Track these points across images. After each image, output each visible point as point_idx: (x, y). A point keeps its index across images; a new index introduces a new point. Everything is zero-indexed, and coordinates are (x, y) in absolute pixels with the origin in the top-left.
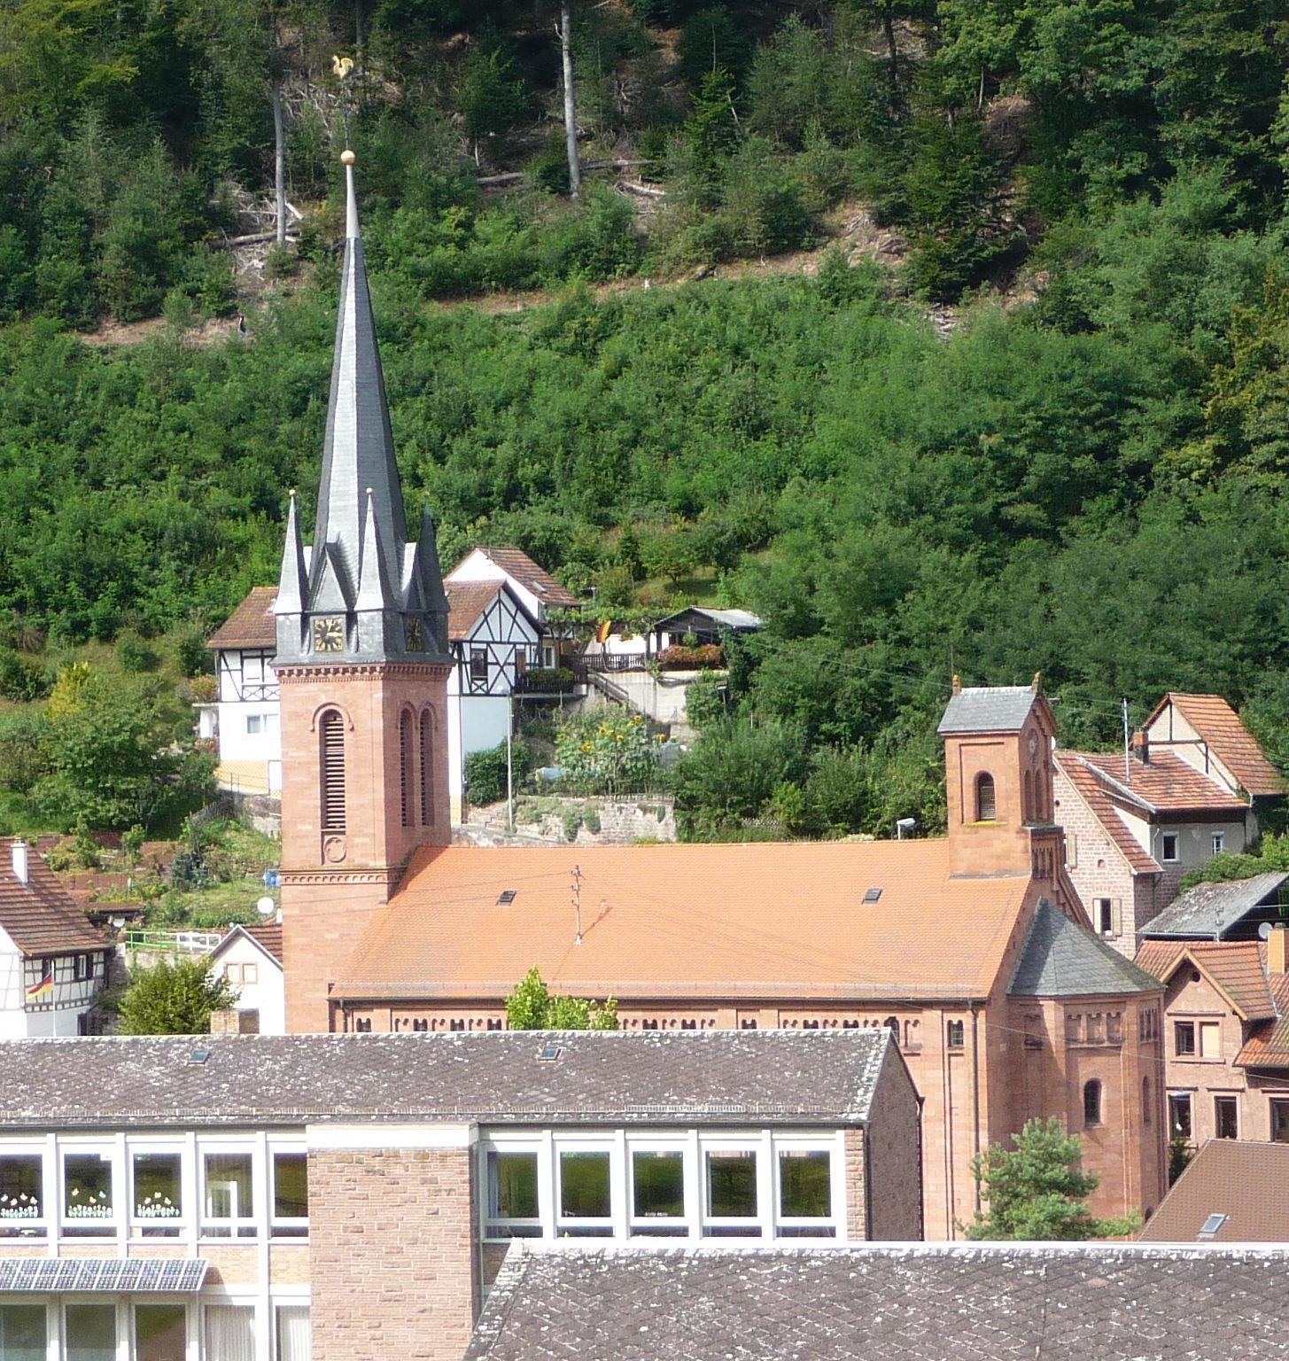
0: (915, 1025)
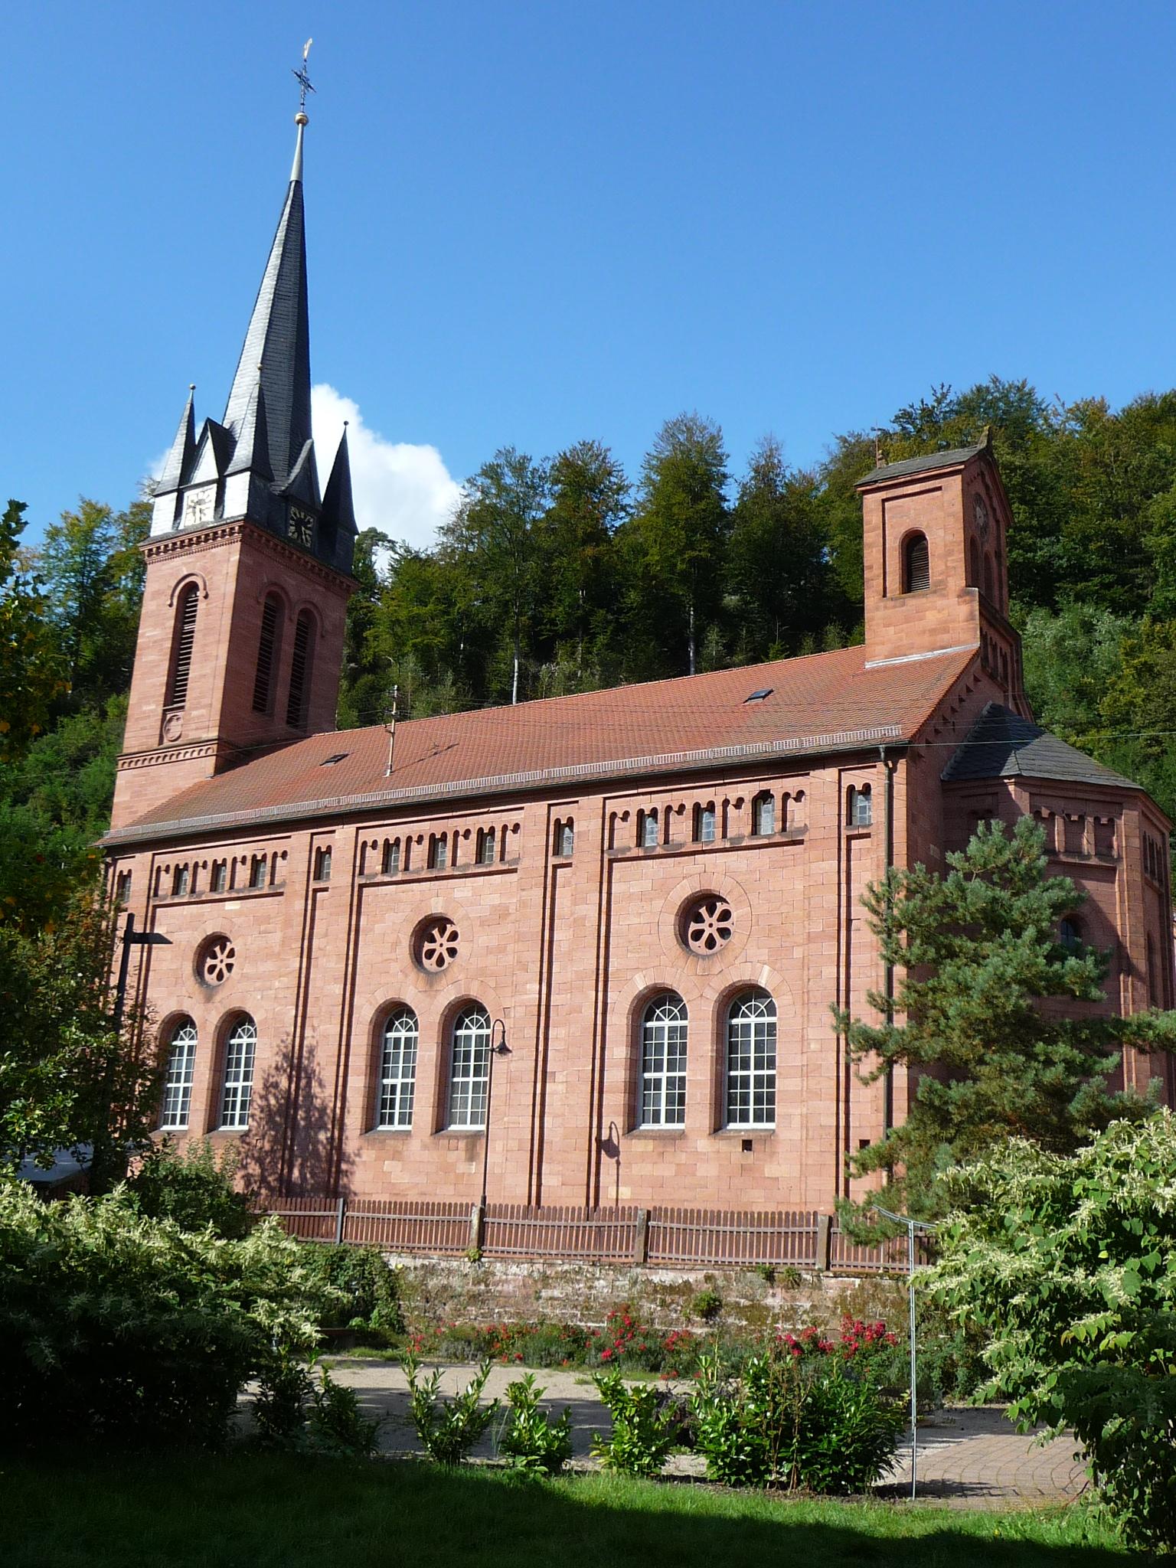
0: (798, 799)
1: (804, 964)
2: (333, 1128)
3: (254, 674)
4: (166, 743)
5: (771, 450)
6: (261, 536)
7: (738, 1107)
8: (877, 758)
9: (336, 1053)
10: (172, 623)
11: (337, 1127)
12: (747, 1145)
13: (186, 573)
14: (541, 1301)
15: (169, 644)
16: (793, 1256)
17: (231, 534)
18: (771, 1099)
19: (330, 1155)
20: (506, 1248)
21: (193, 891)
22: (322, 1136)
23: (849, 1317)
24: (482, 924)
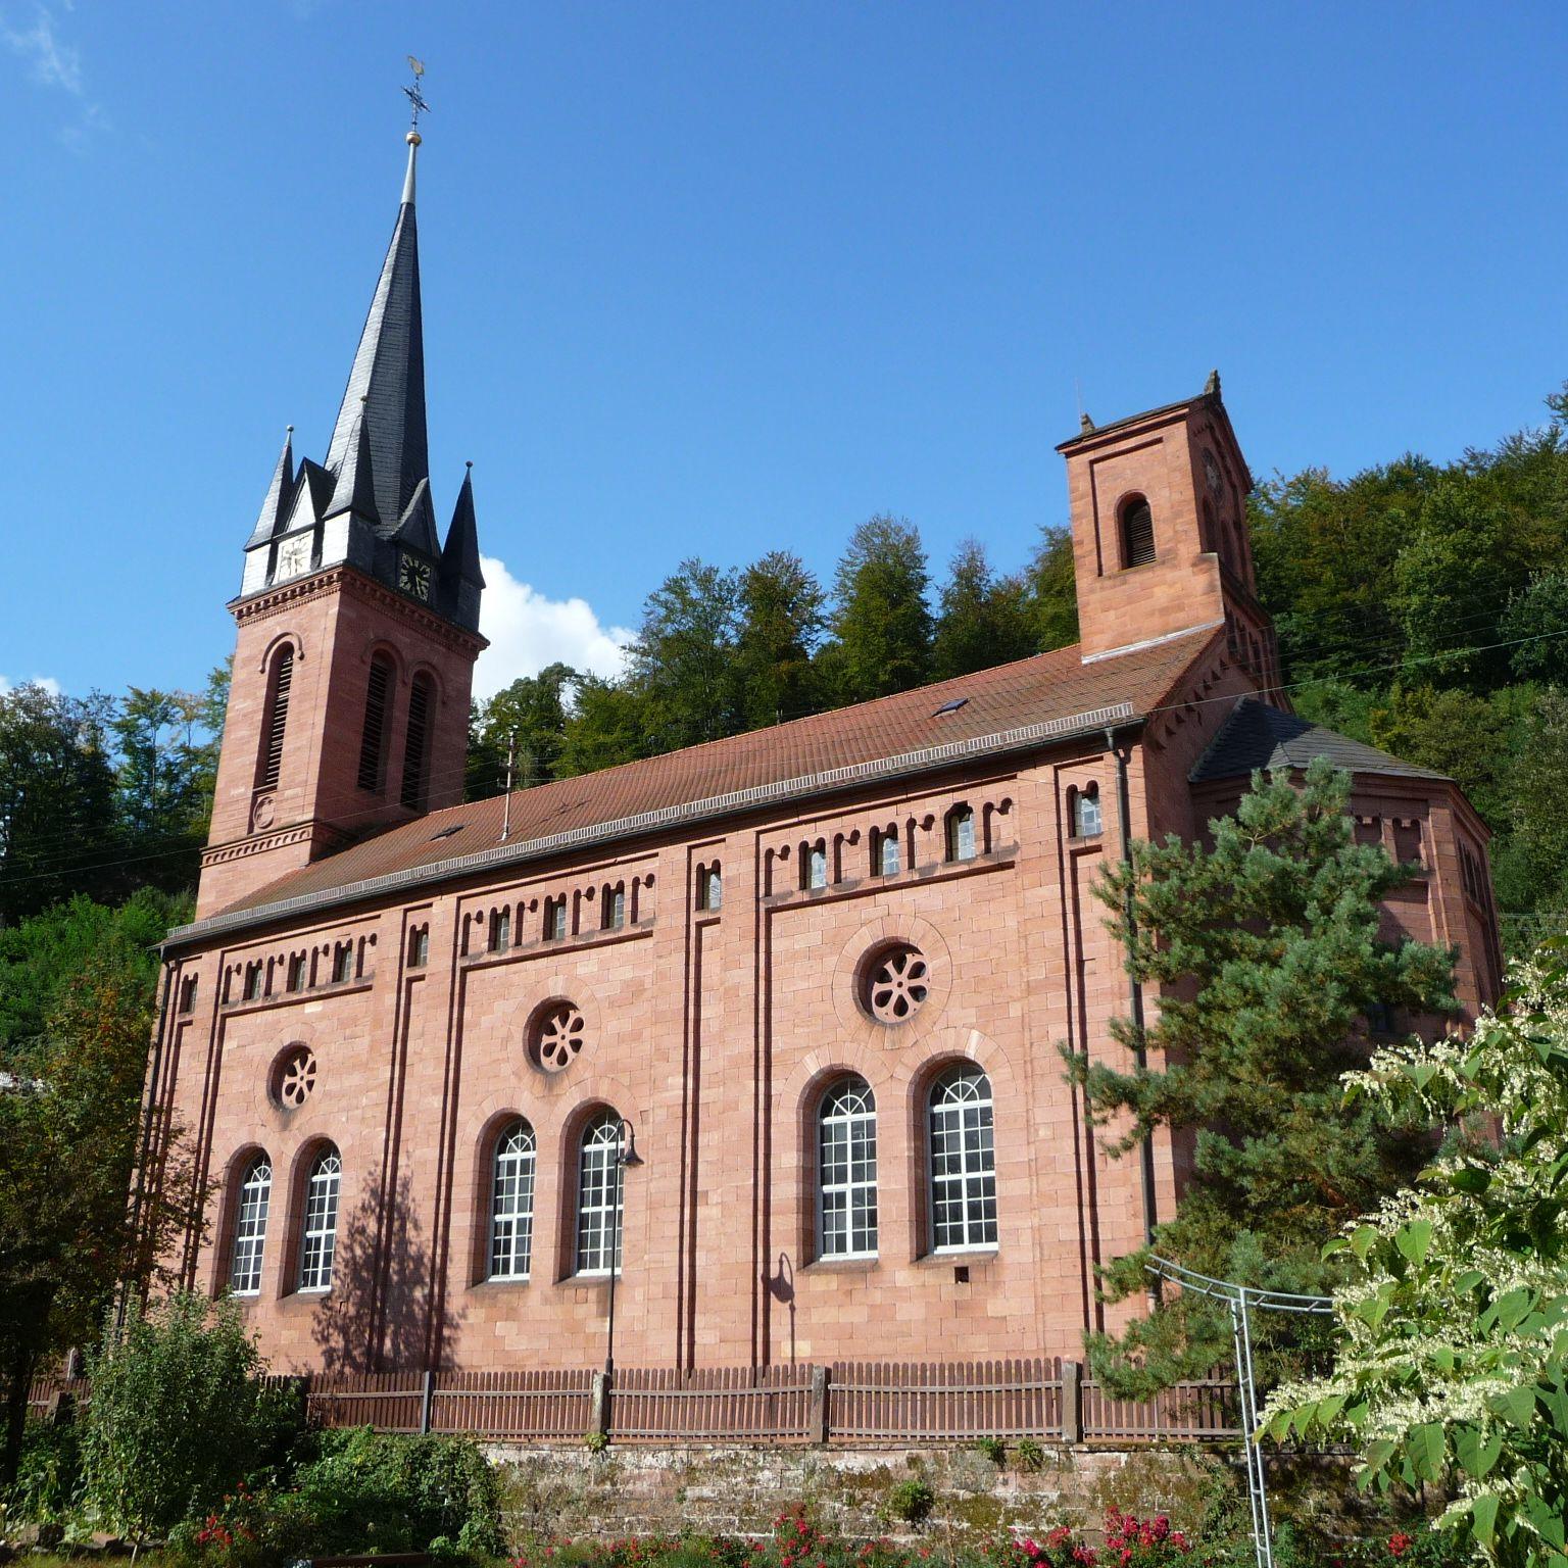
1: (1024, 1023)
2: (432, 1282)
3: (359, 746)
4: (257, 830)
5: (973, 553)
6: (365, 585)
7: (948, 1224)
8: (1104, 747)
9: (435, 1183)
10: (264, 691)
11: (437, 1280)
12: (962, 1274)
13: (279, 633)
14: (685, 1504)
15: (260, 716)
16: (1029, 1424)
17: (330, 583)
18: (991, 1211)
19: (428, 1318)
20: (639, 1431)
21: (268, 993)
22: (419, 1294)
23: (1114, 1511)
24: (611, 1005)
